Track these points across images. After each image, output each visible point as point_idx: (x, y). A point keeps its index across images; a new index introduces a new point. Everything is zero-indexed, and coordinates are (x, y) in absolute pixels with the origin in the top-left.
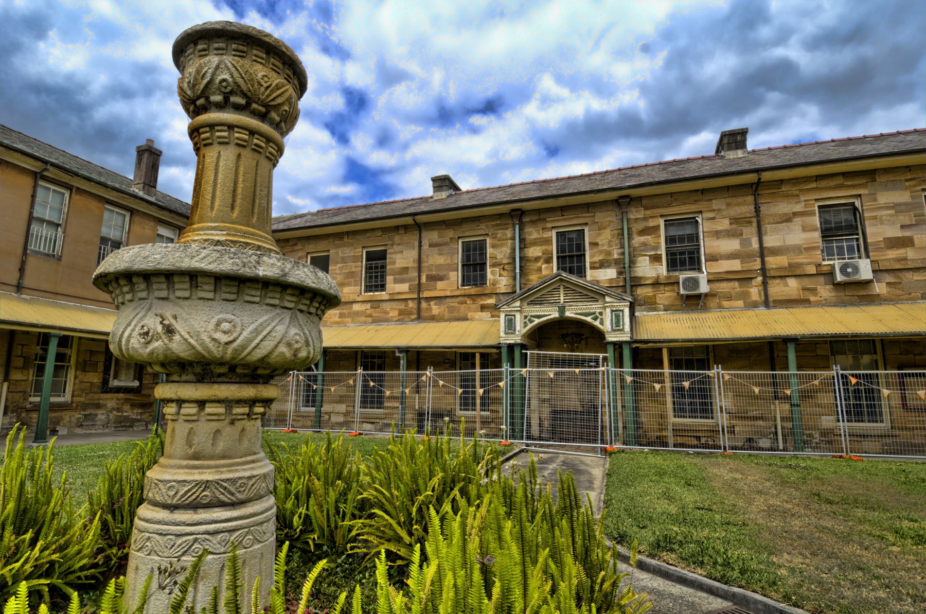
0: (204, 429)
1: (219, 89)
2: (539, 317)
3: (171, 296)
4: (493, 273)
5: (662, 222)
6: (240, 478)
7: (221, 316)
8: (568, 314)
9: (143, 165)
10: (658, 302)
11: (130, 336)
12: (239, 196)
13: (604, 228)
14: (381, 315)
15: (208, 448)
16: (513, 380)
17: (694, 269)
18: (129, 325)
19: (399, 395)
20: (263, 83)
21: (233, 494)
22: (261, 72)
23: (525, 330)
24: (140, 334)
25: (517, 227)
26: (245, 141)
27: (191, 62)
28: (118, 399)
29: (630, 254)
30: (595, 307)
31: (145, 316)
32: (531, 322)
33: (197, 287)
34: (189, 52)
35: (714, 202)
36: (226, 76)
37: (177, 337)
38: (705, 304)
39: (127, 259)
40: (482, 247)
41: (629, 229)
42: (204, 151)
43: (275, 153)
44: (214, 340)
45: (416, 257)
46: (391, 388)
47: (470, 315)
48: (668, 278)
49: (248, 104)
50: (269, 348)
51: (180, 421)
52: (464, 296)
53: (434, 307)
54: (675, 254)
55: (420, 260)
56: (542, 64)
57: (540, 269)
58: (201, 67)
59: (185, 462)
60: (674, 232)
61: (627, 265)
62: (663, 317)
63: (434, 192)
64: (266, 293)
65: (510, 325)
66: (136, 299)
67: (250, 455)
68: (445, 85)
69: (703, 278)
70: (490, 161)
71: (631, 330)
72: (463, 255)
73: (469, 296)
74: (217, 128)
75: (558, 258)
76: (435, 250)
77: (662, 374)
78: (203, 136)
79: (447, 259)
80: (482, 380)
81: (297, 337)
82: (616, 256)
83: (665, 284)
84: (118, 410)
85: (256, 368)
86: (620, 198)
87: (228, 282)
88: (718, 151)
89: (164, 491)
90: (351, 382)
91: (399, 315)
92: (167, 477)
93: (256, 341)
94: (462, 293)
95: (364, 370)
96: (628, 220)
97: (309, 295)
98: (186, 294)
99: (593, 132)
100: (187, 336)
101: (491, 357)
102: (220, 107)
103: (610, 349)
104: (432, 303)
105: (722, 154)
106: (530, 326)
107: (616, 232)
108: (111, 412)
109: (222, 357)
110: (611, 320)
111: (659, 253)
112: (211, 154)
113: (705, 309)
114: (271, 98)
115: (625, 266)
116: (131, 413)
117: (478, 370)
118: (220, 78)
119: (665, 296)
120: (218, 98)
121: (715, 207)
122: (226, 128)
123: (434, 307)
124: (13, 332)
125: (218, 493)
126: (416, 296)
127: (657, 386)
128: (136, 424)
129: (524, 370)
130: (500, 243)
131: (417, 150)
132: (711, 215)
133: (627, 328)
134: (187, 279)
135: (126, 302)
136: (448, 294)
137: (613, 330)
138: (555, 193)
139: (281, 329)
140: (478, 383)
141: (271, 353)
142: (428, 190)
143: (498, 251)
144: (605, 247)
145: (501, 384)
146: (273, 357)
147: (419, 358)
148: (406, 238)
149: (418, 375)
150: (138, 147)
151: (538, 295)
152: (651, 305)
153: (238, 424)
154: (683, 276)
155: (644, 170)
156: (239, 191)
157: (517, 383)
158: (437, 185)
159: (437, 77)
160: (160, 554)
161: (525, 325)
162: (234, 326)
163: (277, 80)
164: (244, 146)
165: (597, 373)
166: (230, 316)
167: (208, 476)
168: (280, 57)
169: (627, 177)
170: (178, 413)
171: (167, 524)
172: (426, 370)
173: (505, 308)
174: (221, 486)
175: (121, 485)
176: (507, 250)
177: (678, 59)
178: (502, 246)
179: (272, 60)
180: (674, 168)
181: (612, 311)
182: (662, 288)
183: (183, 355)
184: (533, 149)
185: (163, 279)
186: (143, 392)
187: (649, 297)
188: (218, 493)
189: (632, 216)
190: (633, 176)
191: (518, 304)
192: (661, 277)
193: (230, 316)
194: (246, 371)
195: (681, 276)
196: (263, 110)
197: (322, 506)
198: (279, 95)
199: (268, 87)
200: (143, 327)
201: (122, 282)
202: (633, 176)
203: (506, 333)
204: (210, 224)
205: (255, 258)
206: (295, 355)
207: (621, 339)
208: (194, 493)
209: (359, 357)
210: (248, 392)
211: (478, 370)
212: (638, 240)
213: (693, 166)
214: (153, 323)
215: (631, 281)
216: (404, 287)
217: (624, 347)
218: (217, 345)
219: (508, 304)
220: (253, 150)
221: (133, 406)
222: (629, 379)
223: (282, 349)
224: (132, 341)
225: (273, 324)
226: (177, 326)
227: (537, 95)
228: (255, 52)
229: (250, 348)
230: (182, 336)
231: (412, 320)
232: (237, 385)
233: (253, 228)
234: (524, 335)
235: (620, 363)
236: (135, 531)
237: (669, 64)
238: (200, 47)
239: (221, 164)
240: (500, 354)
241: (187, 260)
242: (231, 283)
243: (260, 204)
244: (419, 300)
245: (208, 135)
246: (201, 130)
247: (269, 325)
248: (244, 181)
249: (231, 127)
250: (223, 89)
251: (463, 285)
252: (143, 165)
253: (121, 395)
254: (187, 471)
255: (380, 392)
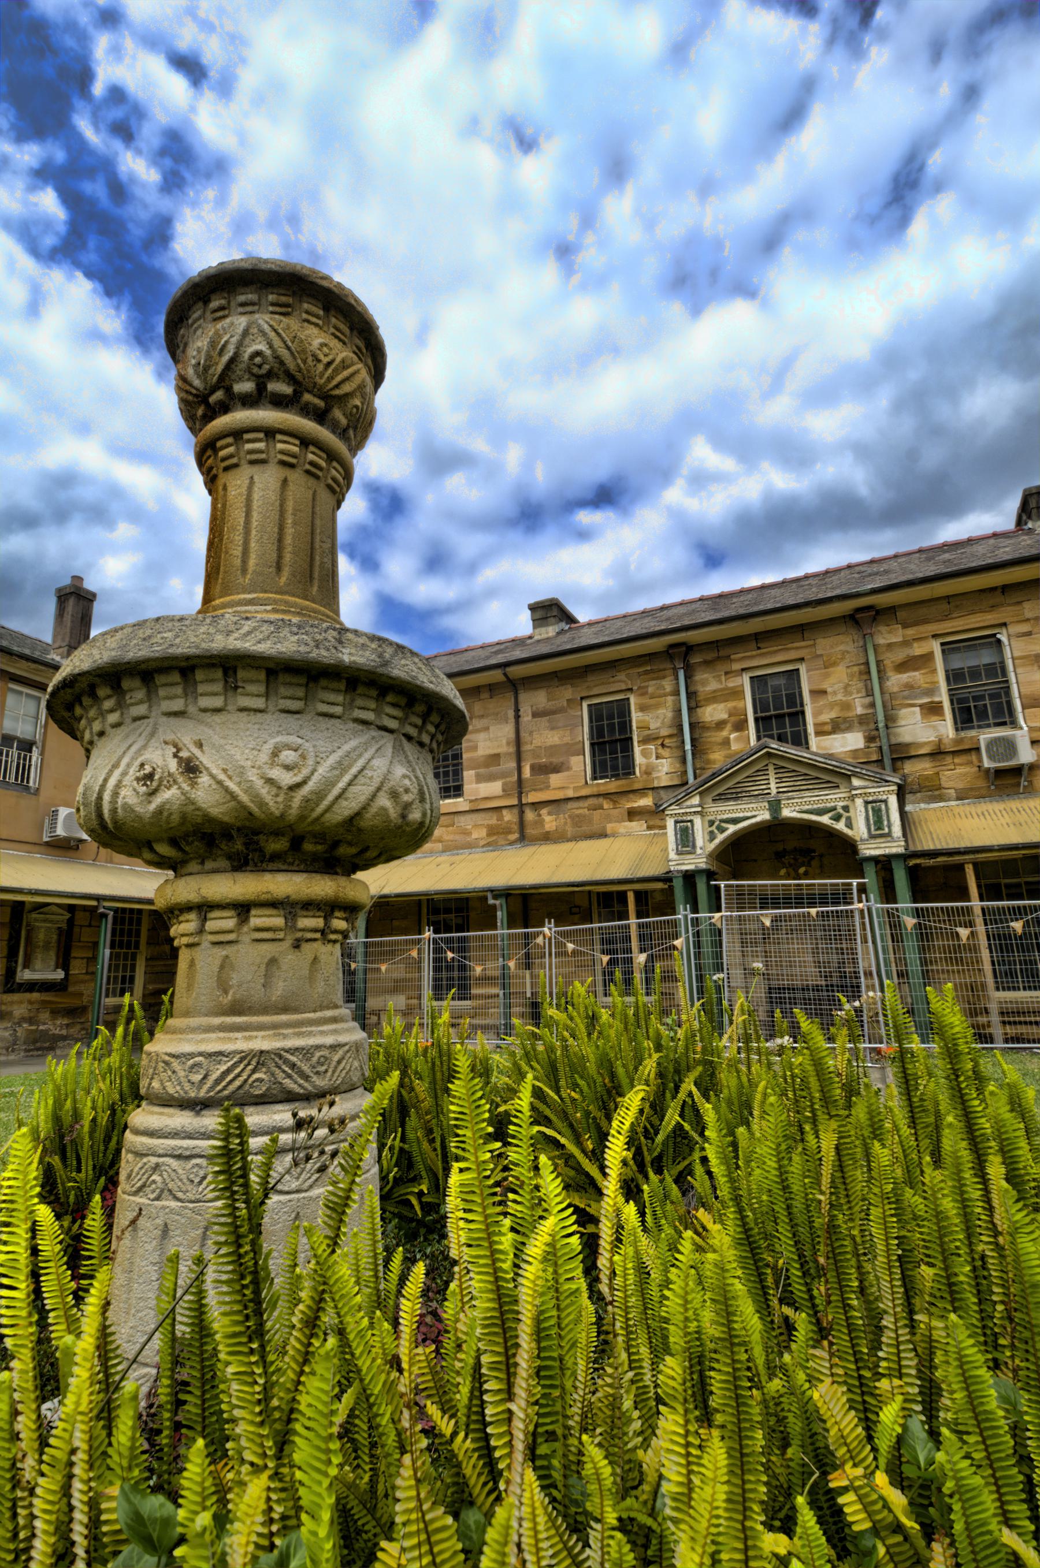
0: (249, 956)
1: (249, 370)
2: (735, 821)
3: (192, 709)
4: (644, 754)
5: (936, 647)
6: (318, 1047)
7: (279, 739)
8: (787, 813)
9: (68, 618)
10: (944, 784)
11: (118, 785)
12: (289, 549)
13: (834, 664)
14: (457, 837)
15: (257, 993)
16: (697, 934)
17: (1004, 724)
18: (116, 766)
19: (498, 973)
20: (321, 357)
21: (306, 1078)
22: (319, 339)
23: (712, 846)
24: (138, 779)
25: (681, 674)
26: (294, 456)
27: (199, 332)
28: (30, 1002)
29: (884, 706)
30: (835, 798)
31: (144, 747)
32: (722, 830)
33: (236, 688)
34: (195, 315)
35: (1027, 605)
36: (262, 347)
37: (204, 779)
38: (1031, 782)
39: (114, 645)
40: (622, 709)
41: (878, 663)
42: (223, 478)
43: (341, 479)
44: (270, 781)
45: (512, 735)
46: (482, 960)
47: (610, 827)
48: (958, 741)
49: (297, 395)
50: (363, 799)
51: (205, 944)
52: (598, 795)
53: (548, 819)
54: (965, 700)
55: (518, 741)
56: (690, 421)
57: (727, 742)
58: (218, 335)
59: (217, 1021)
60: (963, 661)
61: (881, 725)
62: (956, 811)
63: (534, 627)
64: (353, 700)
65: (685, 838)
66: (128, 721)
67: (328, 1008)
68: (528, 465)
69: (1022, 737)
70: (611, 582)
71: (905, 835)
72: (591, 728)
73: (606, 795)
74: (246, 436)
75: (756, 720)
76: (544, 721)
77: (969, 910)
78: (222, 453)
79: (563, 733)
80: (641, 938)
81: (407, 782)
82: (859, 710)
83: (953, 752)
84: (31, 1021)
85: (336, 844)
86: (859, 610)
87: (288, 678)
88: (1019, 522)
89: (182, 1074)
90: (414, 954)
91: (489, 835)
92: (187, 1048)
93: (341, 785)
94: (595, 790)
95: (435, 932)
96: (876, 647)
97: (420, 708)
98: (218, 702)
99: (780, 523)
100: (222, 777)
101: (655, 896)
102: (249, 401)
103: (870, 870)
104: (544, 812)
105: (1030, 525)
106: (720, 837)
107: (856, 669)
108: (19, 1024)
109: (282, 816)
110: (861, 817)
111: (937, 699)
112: (236, 483)
113: (1030, 791)
114: (334, 383)
115: (878, 727)
116: (54, 1026)
117: (633, 921)
118: (250, 350)
119: (956, 775)
120: (245, 386)
121: (1028, 614)
122: (261, 435)
123: (548, 819)
124: (71, 908)
125: (280, 1076)
126: (515, 802)
127: (964, 932)
128: (60, 1044)
129: (717, 915)
130: (653, 701)
131: (488, 575)
132: (1024, 628)
133: (897, 830)
134: (219, 674)
135: (108, 729)
136: (571, 794)
137: (872, 837)
138: (742, 611)
139: (380, 765)
140: (635, 944)
141: (365, 808)
142: (522, 625)
143: (650, 715)
144: (840, 697)
145: (678, 943)
146: (368, 816)
147: (528, 905)
148: (492, 705)
149: (526, 936)
150: (59, 590)
151: (730, 784)
152: (933, 791)
153: (306, 947)
154: (985, 736)
155: (894, 564)
156: (288, 540)
157: (705, 939)
158: (539, 614)
159: (513, 457)
160: (180, 1195)
161: (712, 837)
162: (303, 757)
163: (342, 353)
164: (292, 466)
165: (850, 914)
166: (293, 740)
167: (262, 1042)
168: (345, 316)
169: (864, 577)
170: (201, 931)
171: (190, 1136)
172: (543, 926)
173: (674, 810)
174: (286, 1061)
175: (75, 1101)
176: (665, 713)
177: (915, 400)
178: (657, 706)
179: (333, 320)
180: (947, 556)
181: (867, 803)
182: (949, 759)
183: (215, 812)
184: (681, 556)
185: (176, 677)
186: (71, 989)
187: (927, 778)
188: (280, 1076)
189: (881, 641)
190: (877, 574)
191: (696, 800)
192: (946, 741)
193: (293, 740)
194: (319, 847)
195: (982, 737)
196: (320, 403)
197: (430, 1131)
198: (347, 379)
199: (329, 364)
200: (142, 765)
201: (101, 692)
202: (877, 574)
203: (679, 853)
204: (242, 596)
205: (335, 634)
206: (404, 816)
207: (887, 851)
208: (239, 1075)
209: (424, 910)
210: (322, 887)
211: (633, 921)
212: (896, 680)
213: (980, 549)
214: (161, 759)
215: (892, 752)
216: (495, 788)
217: (894, 865)
218: (274, 791)
219: (678, 802)
220: (308, 472)
221: (55, 1013)
222: (910, 922)
223: (384, 801)
224: (123, 792)
225: (367, 755)
226: (205, 759)
227: (685, 471)
228: (306, 306)
229: (330, 798)
230: (213, 776)
231: (511, 843)
232: (305, 875)
233: (313, 601)
234: (710, 856)
235: (889, 894)
236: (126, 1157)
237: (898, 407)
238: (214, 304)
239: (256, 496)
240: (671, 889)
241: (219, 637)
242: (295, 680)
243: (322, 563)
244: (521, 807)
245: (231, 450)
246: (219, 444)
247: (360, 756)
248: (295, 523)
249: (270, 433)
250: (255, 370)
251: (594, 778)
252: (68, 618)
253: (35, 996)
254: (222, 1035)
255: (463, 968)
